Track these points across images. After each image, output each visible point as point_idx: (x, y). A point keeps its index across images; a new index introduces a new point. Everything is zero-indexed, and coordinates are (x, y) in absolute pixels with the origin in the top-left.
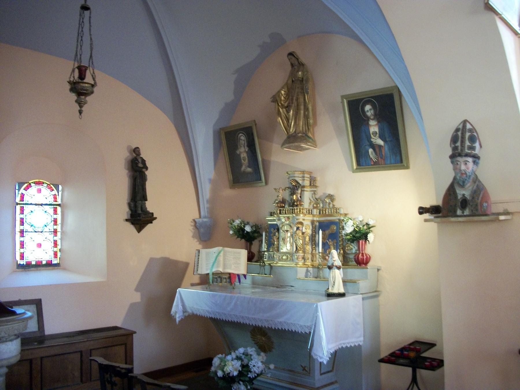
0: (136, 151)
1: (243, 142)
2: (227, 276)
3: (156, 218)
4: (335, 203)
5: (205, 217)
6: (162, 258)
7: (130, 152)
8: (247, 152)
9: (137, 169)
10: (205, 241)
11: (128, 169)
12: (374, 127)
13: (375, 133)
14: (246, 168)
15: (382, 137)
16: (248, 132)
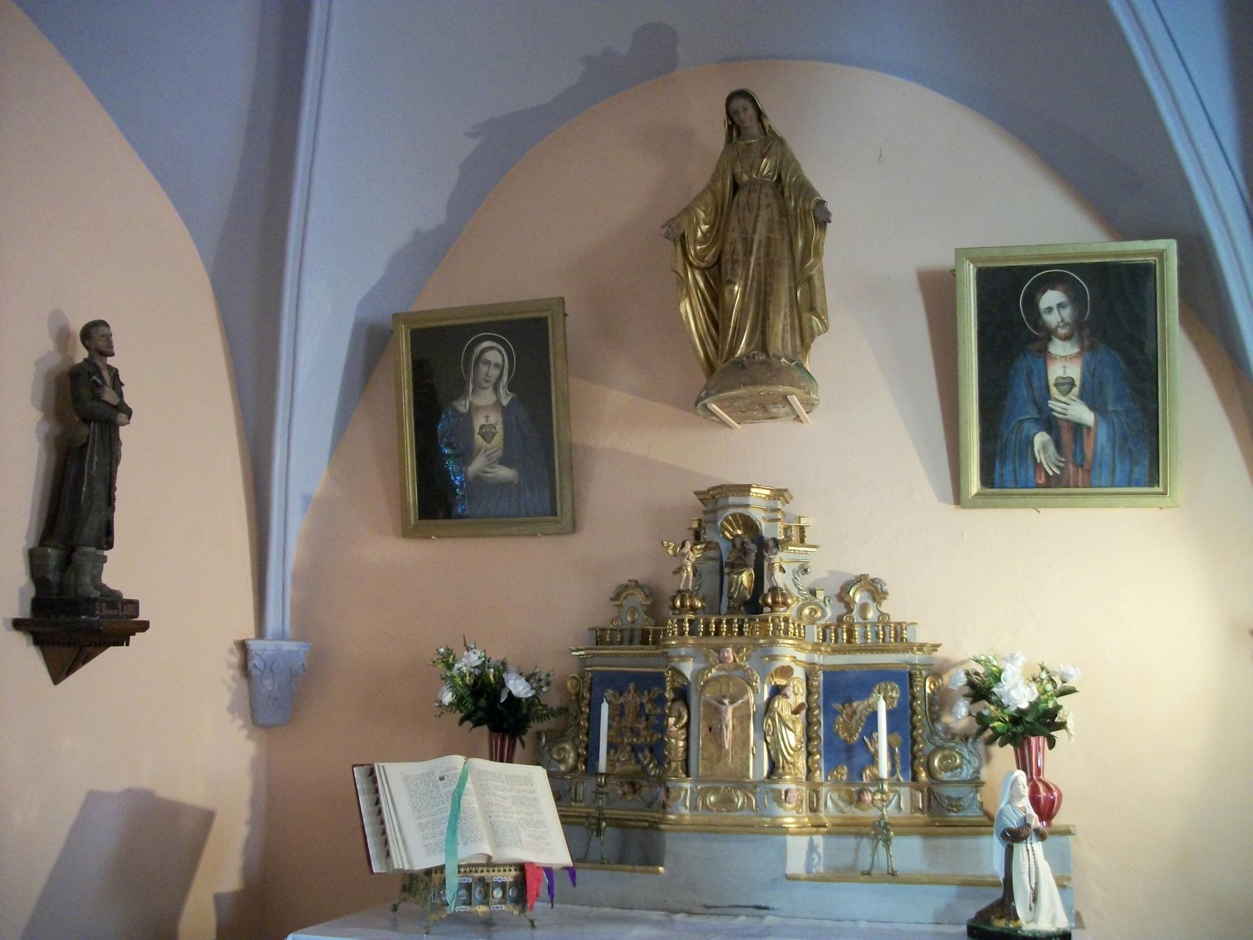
0: (95, 335)
1: (495, 373)
2: (509, 876)
3: (144, 626)
5: (283, 637)
6: (130, 791)
7: (63, 337)
8: (506, 412)
9: (85, 412)
10: (267, 727)
11: (44, 408)
12: (1065, 363)
13: (1066, 384)
14: (487, 461)
15: (1090, 396)
16: (530, 338)
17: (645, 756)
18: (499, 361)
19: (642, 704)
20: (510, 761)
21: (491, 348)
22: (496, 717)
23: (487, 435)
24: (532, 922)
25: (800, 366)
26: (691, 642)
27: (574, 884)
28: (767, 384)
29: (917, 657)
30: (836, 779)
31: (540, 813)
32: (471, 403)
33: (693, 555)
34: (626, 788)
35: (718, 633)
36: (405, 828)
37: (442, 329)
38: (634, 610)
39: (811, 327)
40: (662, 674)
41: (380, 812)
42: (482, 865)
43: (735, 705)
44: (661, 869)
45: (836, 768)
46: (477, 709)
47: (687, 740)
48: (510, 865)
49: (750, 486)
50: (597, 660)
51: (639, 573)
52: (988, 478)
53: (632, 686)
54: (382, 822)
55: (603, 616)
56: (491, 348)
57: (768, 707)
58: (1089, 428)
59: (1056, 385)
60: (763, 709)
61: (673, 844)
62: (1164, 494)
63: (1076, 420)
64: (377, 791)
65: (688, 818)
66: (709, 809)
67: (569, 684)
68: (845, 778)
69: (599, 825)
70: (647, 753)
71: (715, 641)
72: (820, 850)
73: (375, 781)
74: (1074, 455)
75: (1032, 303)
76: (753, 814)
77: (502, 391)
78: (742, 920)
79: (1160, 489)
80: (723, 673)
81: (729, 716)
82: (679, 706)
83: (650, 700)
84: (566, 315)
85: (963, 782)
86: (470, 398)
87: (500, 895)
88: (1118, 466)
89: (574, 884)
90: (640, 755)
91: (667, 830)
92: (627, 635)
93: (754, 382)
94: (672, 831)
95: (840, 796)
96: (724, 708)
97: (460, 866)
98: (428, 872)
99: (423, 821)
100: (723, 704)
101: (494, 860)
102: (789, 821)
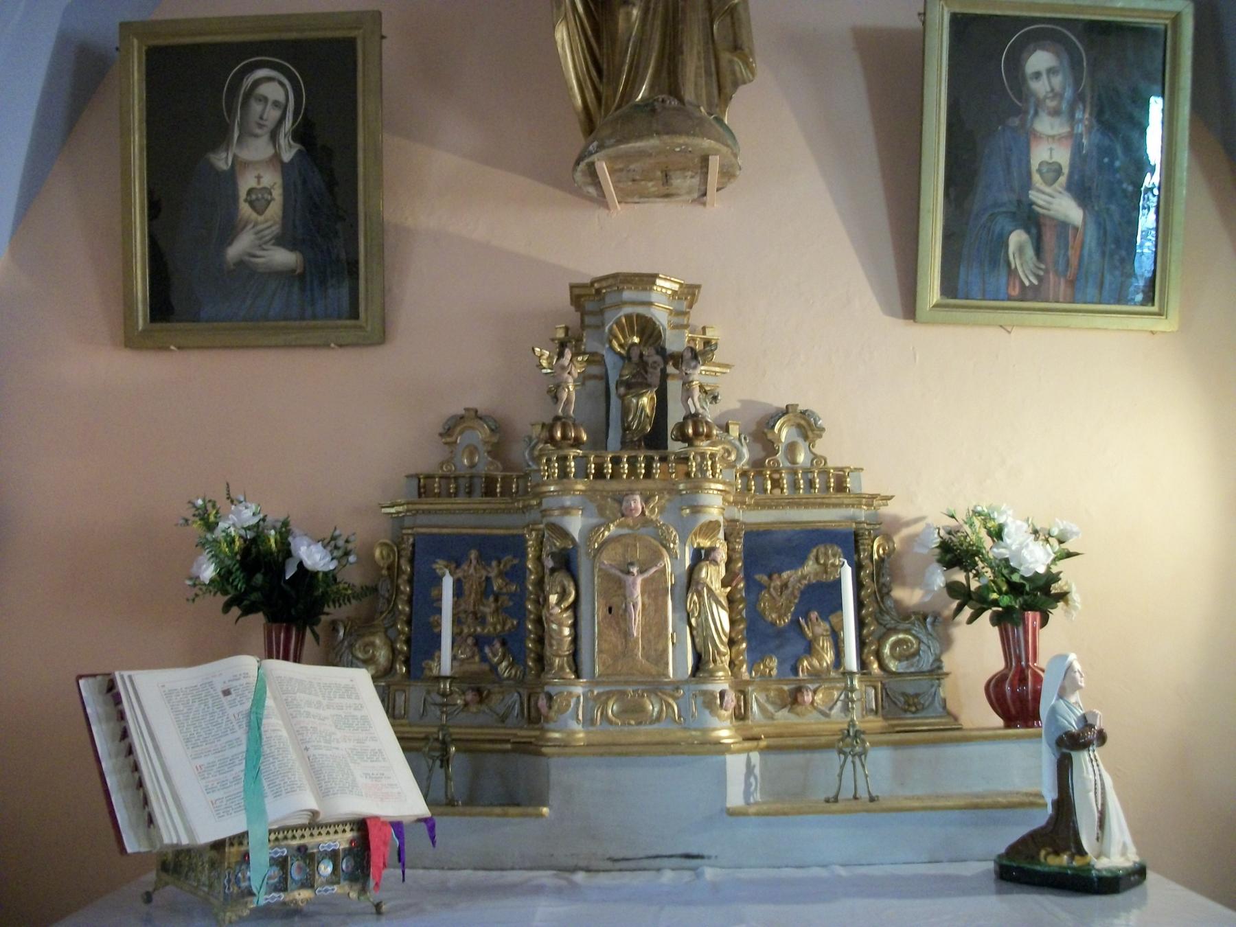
1: (273, 114)
2: (342, 840)
3: (1063, 596)
4: (820, 447)
8: (285, 169)
14: (258, 238)
15: (1081, 191)
17: (495, 652)
18: (282, 98)
19: (488, 579)
20: (297, 659)
21: (270, 79)
22: (277, 599)
23: (258, 201)
24: (378, 906)
25: (719, 120)
26: (580, 487)
27: (434, 843)
28: (688, 134)
29: (862, 513)
30: (763, 675)
31: (374, 739)
32: (235, 157)
33: (574, 368)
34: (470, 696)
35: (616, 475)
36: (177, 779)
37: (195, 49)
38: (472, 450)
39: (733, 73)
40: (523, 536)
41: (130, 751)
42: (303, 827)
43: (646, 575)
44: (545, 810)
45: (762, 660)
46: (251, 589)
47: (575, 626)
48: (344, 823)
49: (655, 276)
50: (422, 519)
51: (479, 400)
52: (949, 288)
53: (473, 555)
54: (136, 768)
55: (428, 460)
56: (270, 79)
57: (691, 580)
58: (1076, 229)
59: (1039, 171)
60: (685, 580)
61: (562, 774)
62: (1160, 314)
63: (1061, 217)
64: (122, 716)
65: (581, 735)
66: (610, 722)
67: (377, 553)
68: (774, 672)
69: (445, 750)
70: (497, 645)
71: (615, 486)
72: (757, 771)
73: (117, 700)
74: (1056, 263)
75: (1016, 64)
76: (674, 727)
77: (283, 141)
78: (668, 876)
79: (1155, 309)
80: (625, 531)
81: (638, 591)
82: (562, 578)
83: (501, 574)
84: (383, 37)
85: (921, 673)
86: (234, 149)
87: (330, 869)
88: (1108, 278)
89: (434, 843)
90: (487, 650)
91: (553, 755)
92: (463, 483)
93: (670, 131)
94: (559, 755)
95: (768, 700)
96: (630, 579)
97: (270, 832)
98: (218, 846)
99: (202, 761)
100: (629, 573)
101: (322, 818)
102: (725, 733)
